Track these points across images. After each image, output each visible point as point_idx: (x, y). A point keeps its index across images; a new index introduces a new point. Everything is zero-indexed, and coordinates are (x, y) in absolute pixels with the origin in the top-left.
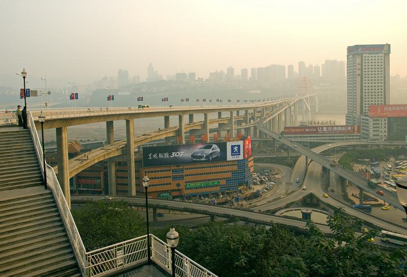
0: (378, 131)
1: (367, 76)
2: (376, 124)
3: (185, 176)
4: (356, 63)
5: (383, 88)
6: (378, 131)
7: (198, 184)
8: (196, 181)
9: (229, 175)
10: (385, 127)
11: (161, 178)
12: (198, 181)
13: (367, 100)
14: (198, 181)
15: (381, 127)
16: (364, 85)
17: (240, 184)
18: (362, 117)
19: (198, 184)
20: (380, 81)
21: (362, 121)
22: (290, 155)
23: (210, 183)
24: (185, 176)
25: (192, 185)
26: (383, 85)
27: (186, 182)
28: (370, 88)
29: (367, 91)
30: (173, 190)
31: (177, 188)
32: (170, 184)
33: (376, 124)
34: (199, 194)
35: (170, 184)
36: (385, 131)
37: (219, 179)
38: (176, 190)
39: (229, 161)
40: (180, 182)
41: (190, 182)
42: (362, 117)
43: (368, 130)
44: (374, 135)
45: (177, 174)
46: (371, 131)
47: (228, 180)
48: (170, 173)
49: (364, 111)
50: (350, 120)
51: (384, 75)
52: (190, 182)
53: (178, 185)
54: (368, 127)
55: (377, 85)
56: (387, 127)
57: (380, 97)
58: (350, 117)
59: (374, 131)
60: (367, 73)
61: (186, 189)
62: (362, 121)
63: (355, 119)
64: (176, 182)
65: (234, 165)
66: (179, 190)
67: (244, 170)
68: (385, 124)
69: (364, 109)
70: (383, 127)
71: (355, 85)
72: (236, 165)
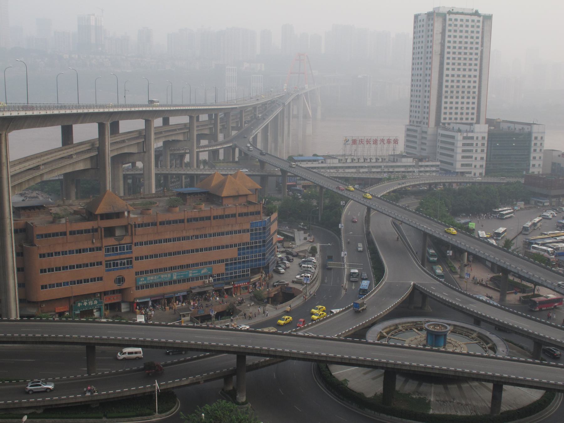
0: (471, 157)
1: (451, 56)
2: (468, 145)
3: (137, 259)
4: (432, 30)
5: (477, 79)
6: (471, 157)
7: (165, 276)
8: (161, 270)
9: (233, 253)
10: (482, 151)
11: (79, 266)
12: (165, 269)
13: (449, 100)
14: (165, 269)
15: (476, 151)
16: (445, 72)
17: (255, 271)
18: (441, 132)
19: (165, 276)
20: (473, 67)
21: (439, 144)
22: (104, 245)
23: (191, 273)
24: (137, 259)
25: (152, 278)
26: (477, 73)
27: (137, 273)
28: (455, 79)
29: (449, 84)
30: (105, 293)
31: (116, 287)
32: (100, 279)
33: (468, 145)
34: (166, 296)
35: (100, 279)
36: (482, 158)
37: (210, 263)
38: (113, 292)
39: (117, 236)
40: (124, 273)
41: (147, 272)
42: (441, 132)
43: (452, 156)
44: (463, 165)
45: (117, 257)
46: (459, 157)
47: (229, 263)
48: (100, 256)
49: (443, 121)
50: (415, 137)
51: (482, 52)
52: (147, 272)
53: (120, 280)
54: (452, 156)
55: (468, 56)
56: (485, 151)
57: (471, 95)
58: (416, 131)
59: (463, 157)
60: (451, 50)
61: (138, 288)
62: (439, 144)
63: (424, 141)
64: (115, 274)
65: (244, 231)
66: (121, 291)
67: (264, 241)
68: (483, 144)
69: (443, 116)
70: (479, 150)
71: (428, 72)
72: (248, 231)
